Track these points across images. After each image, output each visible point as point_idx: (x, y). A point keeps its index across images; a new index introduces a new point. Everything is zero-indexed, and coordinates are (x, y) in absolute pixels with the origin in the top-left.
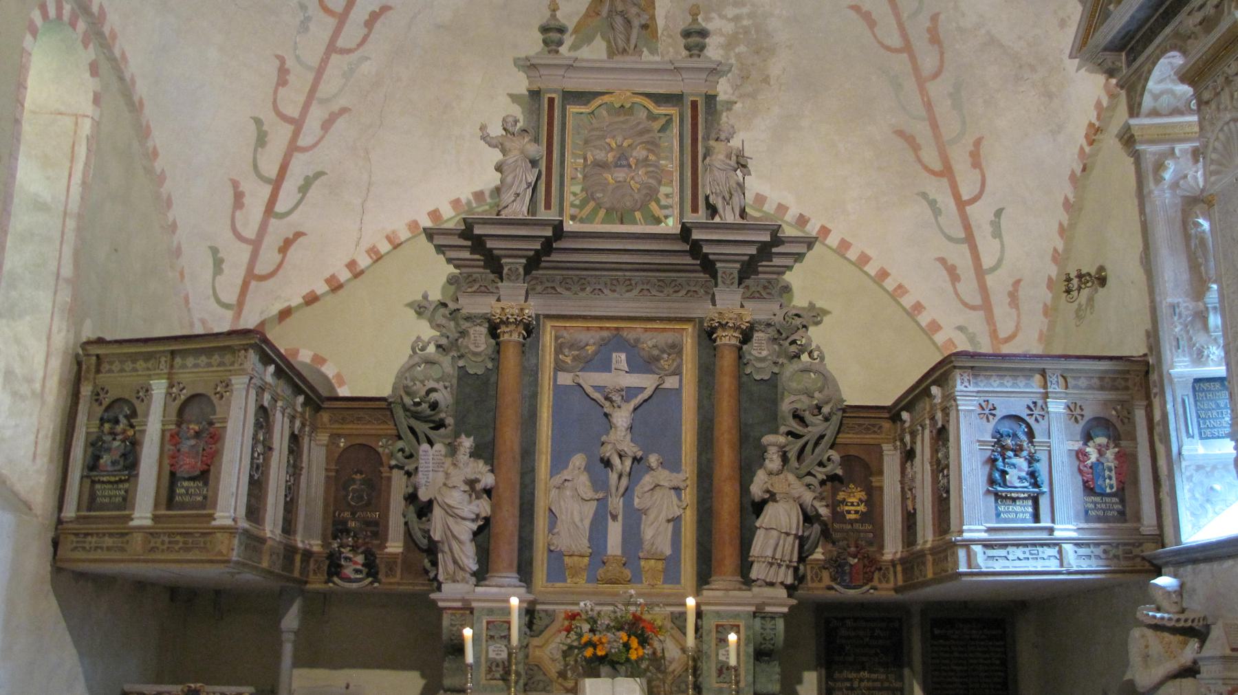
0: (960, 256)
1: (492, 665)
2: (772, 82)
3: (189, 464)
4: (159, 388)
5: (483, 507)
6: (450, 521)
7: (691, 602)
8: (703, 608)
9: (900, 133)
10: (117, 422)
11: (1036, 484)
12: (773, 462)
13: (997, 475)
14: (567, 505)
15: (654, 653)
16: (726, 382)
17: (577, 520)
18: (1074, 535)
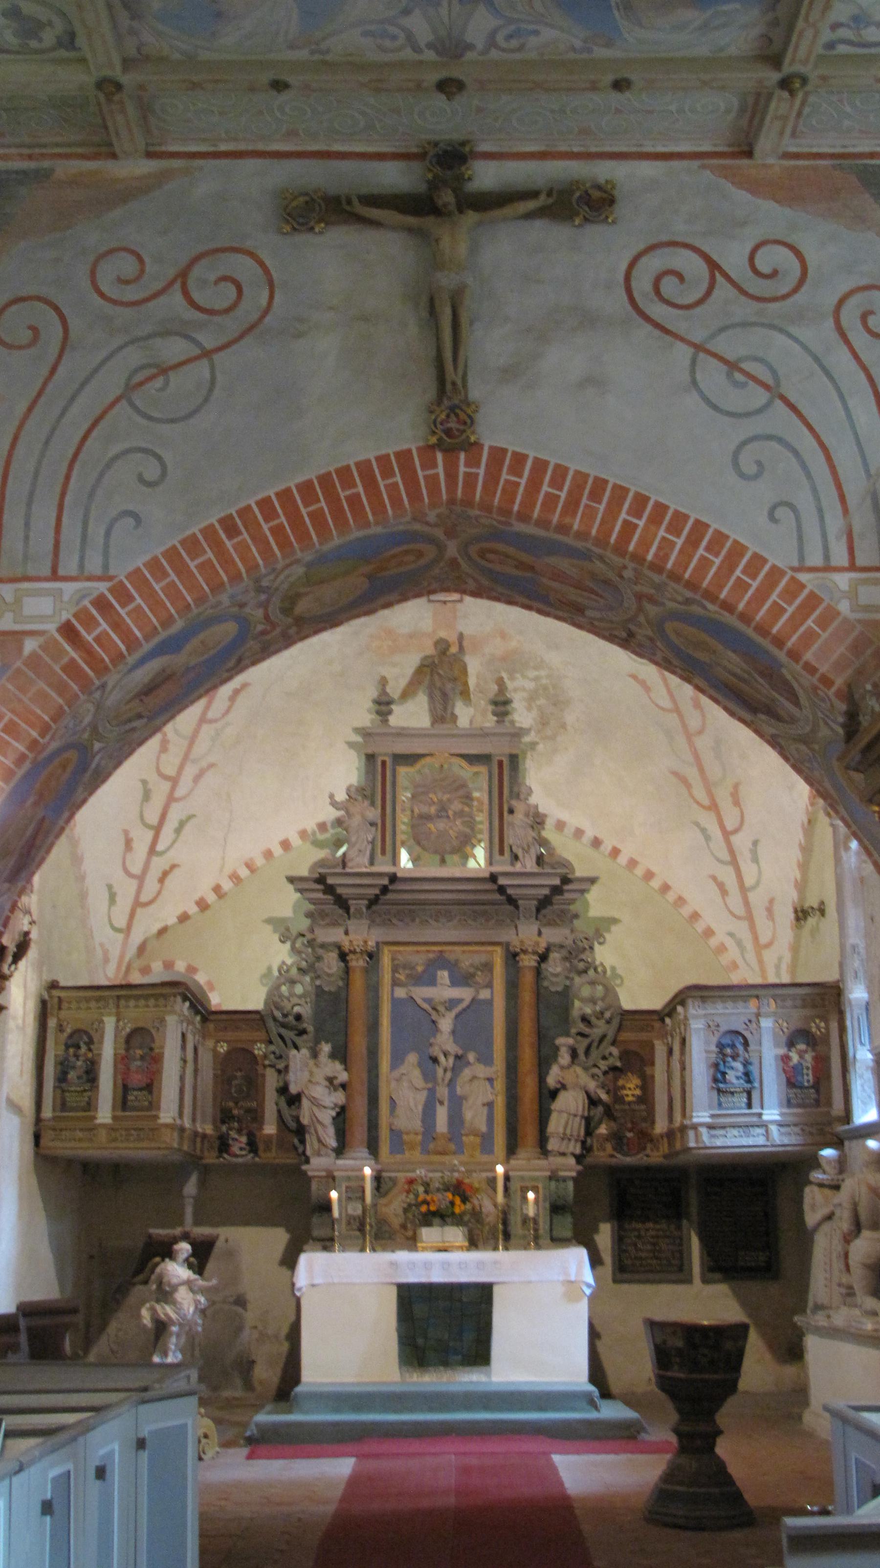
0: (727, 875)
1: (350, 1220)
2: (569, 728)
3: (137, 1079)
4: (110, 1023)
5: (339, 1097)
6: (315, 1109)
7: (500, 1169)
8: (511, 1174)
9: (675, 774)
10: (78, 1047)
11: (749, 1081)
12: (564, 1058)
13: (719, 1076)
14: (404, 1092)
15: (473, 1209)
16: (527, 996)
17: (412, 1104)
18: (778, 1118)
